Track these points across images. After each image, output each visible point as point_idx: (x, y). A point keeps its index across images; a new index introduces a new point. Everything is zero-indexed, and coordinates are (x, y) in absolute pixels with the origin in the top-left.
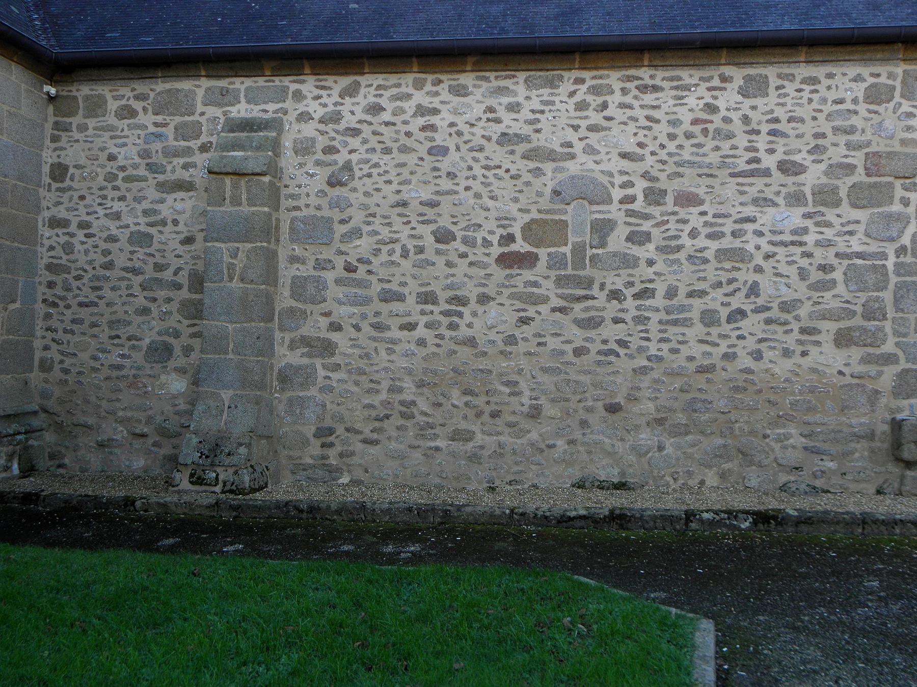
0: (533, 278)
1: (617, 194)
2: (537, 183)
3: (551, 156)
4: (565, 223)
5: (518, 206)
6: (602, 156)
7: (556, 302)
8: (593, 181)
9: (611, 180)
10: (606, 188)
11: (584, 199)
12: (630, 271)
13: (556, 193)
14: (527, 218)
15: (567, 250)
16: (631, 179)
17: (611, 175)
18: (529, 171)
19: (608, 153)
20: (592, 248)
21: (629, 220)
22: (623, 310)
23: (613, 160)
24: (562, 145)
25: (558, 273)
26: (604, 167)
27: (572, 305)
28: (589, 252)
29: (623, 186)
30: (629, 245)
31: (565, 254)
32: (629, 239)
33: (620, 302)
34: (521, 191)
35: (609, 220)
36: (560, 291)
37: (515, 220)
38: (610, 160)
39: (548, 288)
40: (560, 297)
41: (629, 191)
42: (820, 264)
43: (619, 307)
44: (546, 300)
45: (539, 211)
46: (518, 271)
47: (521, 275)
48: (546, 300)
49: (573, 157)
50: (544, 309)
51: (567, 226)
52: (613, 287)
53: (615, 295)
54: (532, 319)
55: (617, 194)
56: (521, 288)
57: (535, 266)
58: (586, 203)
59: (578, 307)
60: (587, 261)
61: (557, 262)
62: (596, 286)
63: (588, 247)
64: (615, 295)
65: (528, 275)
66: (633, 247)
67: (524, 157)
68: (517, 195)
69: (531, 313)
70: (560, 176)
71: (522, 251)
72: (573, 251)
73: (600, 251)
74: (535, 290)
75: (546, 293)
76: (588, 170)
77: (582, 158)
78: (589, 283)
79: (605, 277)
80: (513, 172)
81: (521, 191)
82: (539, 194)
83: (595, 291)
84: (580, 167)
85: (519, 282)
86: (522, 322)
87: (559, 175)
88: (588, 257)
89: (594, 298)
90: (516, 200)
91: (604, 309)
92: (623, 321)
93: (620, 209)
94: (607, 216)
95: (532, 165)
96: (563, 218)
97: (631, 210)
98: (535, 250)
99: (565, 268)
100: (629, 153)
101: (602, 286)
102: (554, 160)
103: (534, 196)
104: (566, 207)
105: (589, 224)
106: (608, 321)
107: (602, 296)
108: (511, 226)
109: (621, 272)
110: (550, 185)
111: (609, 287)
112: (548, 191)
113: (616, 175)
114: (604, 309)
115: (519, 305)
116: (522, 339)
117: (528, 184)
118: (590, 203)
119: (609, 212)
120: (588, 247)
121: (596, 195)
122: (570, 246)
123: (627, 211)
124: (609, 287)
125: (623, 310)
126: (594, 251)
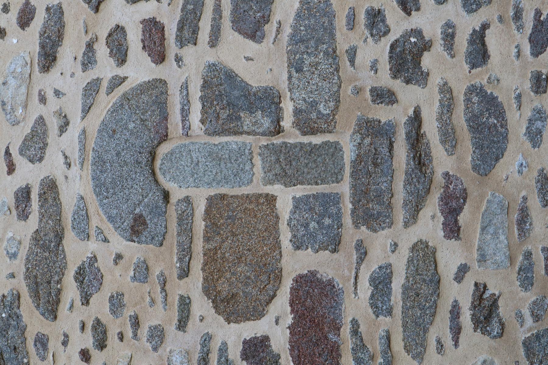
0: (365, 289)
1: (140, 69)
2: (117, 278)
3: (48, 246)
4: (213, 202)
5: (171, 329)
6: (48, 111)
7: (429, 225)
8: (108, 130)
9: (105, 84)
10: (125, 97)
11: (153, 156)
12: (341, 22)
13: (137, 229)
14: (201, 306)
15: (285, 197)
16: (103, 34)
17: (92, 90)
18: (86, 301)
19: (43, 100)
20: (278, 130)
21: (204, 35)
22: (449, 37)
23: (59, 84)
24: (24, 215)
25: (348, 220)
26: (73, 105)
27: (439, 178)
28: (293, 137)
29: (120, 55)
30: (270, 29)
31: (298, 203)
32: (254, 33)
33: (427, 46)
34: (136, 323)
35: (206, 85)
36: (400, 215)
37: (207, 339)
38: (57, 93)
39: (390, 247)
40: (413, 218)
41: (134, 38)
42: (177, 329)
43: (438, 47)
44: (424, 256)
45: (184, 273)
46: (346, 331)
47: (355, 323)
48: (424, 256)
49: (50, 187)
50: (450, 256)
51: (223, 197)
52: (385, 66)
53: (407, 60)
54: (480, 289)
55: (140, 69)
56: (394, 324)
57: (331, 283)
58: (164, 149)
59: (442, 162)
60: (317, 140)
61: (320, 226)
62: (383, 114)
63: (277, 140)
64: (407, 60)
65: (356, 305)
66: (276, 18)
67: (52, 311)
68: (144, 332)
69: (461, 294)
70: (98, 219)
71: (289, 320)
72: (288, 180)
73: (288, 107)
74: (397, 285)
75: (404, 252)
76: (83, 149)
77: (53, 165)
78: (375, 132)
79: (358, 91)
80: (87, 341)
81: (136, 323)
82: (142, 271)
83: (396, 115)
84: (75, 169)
85: (374, 328)
86: (488, 318)
87: (95, 222)
88: (306, 139)
89: (416, 119)
90: (158, 336)
91: (446, 89)
92: (479, 39)
93: (178, 59)
94: (196, 92)
95: (71, 291)
96: (200, 208)
97: (180, 29)
98: (287, 284)
99: (334, 200)
100: (43, 46)
101: (385, 96)
102: (59, 237)
103: (146, 287)
104: (173, 200)
105: (217, 140)
106: (480, 76)
107: (409, 96)
108: (223, 349)
109: (342, 46)
110: (119, 243)
111: (385, 79)
112: (134, 251)
113: (92, 74)
114: (446, 89)
115: (440, 328)
116: (537, 318)
117: (117, 303)
118: (164, 138)
119: (185, 87)
120: (277, 140)
121: (139, 132)
122: (276, 189)
123: (181, 42)
124: (385, 79)
125: (449, 37)
126: (287, 123)
